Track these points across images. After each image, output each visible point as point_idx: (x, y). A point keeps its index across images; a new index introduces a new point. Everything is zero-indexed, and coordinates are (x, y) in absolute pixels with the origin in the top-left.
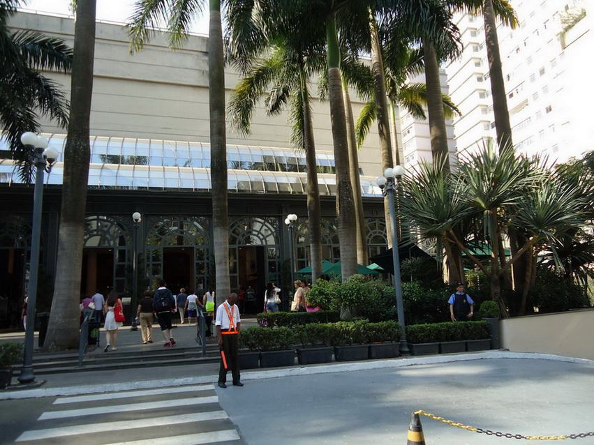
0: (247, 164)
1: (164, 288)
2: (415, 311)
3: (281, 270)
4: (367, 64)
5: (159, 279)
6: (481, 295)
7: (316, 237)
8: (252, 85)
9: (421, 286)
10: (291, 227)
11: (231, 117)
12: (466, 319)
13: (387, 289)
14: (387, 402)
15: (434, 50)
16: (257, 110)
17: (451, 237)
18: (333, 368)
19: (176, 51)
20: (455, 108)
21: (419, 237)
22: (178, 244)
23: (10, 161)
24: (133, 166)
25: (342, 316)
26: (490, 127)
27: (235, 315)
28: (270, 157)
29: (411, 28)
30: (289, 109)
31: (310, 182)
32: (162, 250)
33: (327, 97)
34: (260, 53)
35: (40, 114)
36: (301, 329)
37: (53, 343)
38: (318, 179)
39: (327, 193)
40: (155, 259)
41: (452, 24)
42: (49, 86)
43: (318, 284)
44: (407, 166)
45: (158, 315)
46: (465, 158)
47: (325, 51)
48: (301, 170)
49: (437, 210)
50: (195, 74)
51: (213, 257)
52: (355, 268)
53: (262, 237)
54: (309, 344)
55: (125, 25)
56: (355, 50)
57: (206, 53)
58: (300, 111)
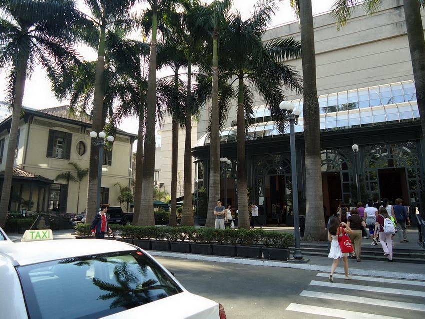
19: (373, 15)
22: (389, 166)
23: (272, 123)
35: (285, 90)
37: (309, 236)
42: (288, 70)
50: (389, 28)
55: (331, 12)
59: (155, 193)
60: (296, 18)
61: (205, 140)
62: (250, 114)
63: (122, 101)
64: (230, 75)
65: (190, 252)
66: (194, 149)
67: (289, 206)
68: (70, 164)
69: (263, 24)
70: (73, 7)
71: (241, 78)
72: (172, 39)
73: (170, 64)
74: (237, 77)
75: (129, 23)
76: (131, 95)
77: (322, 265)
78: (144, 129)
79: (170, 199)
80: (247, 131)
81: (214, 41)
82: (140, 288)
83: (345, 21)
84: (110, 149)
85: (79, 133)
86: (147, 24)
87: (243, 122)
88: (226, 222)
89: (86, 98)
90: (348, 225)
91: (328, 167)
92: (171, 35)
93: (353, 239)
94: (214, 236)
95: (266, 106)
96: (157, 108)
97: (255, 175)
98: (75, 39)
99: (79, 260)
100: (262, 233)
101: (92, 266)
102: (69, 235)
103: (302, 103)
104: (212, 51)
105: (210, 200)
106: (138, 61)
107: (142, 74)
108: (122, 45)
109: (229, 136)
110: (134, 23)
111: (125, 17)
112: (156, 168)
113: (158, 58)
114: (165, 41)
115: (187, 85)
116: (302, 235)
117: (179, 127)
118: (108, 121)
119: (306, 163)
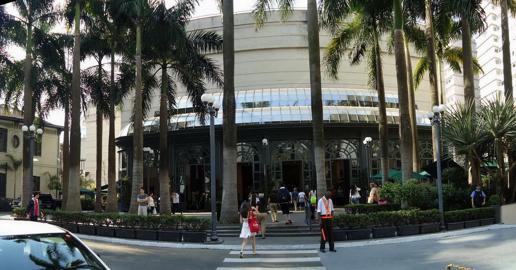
0: (336, 101)
1: (284, 188)
2: (450, 202)
3: (361, 176)
4: (422, 28)
5: (280, 182)
6: (490, 192)
7: (385, 153)
8: (339, 43)
9: (454, 186)
10: (367, 146)
11: (324, 68)
12: (481, 206)
13: (432, 188)
14: (430, 261)
15: (468, 25)
16: (343, 62)
17: (474, 155)
18: (396, 240)
19: (286, 23)
20: (480, 68)
21: (454, 154)
23: (194, 114)
24: (261, 108)
25: (403, 206)
26: (501, 84)
27: (330, 206)
28: (353, 96)
29: (453, 5)
30: (365, 61)
31: (381, 115)
32: (281, 163)
33: (393, 52)
34: (345, 18)
35: (207, 82)
36: (374, 216)
37: (225, 220)
38: (387, 112)
39: (393, 122)
40: (277, 169)
41: (481, 8)
42: (210, 63)
43: (386, 185)
44: (448, 105)
45: (280, 205)
46: (485, 103)
47: (392, 16)
48: (375, 106)
49: (466, 136)
50: (298, 38)
51: (315, 167)
52: (412, 175)
53: (347, 153)
54: (380, 225)
55: (251, 12)
56: (414, 17)
57: (306, 22)
58: (374, 61)
59: (81, 181)
60: (219, 12)
61: (129, 130)
62: (173, 105)
63: (49, 95)
64: (154, 64)
65: (115, 236)
66: (117, 139)
67: (207, 193)
68: (7, 155)
69: (187, 13)
70: (3, 12)
71: (164, 68)
72: (95, 28)
73: (94, 54)
74: (160, 66)
75: (53, 16)
76: (57, 88)
77: (234, 244)
78: (70, 121)
79: (95, 187)
80: (169, 121)
81: (138, 29)
82: (70, 266)
83: (262, 23)
84: (39, 141)
85: (12, 128)
86: (70, 16)
87: (166, 112)
88: (148, 208)
89: (17, 95)
90: (256, 209)
91: (243, 158)
92: (94, 24)
93: (260, 220)
94: (137, 222)
95: (189, 97)
96: (82, 99)
97: (177, 164)
98: (6, 41)
99: (17, 238)
100: (183, 219)
101: (28, 244)
102: (9, 216)
103: (222, 97)
104: (135, 39)
105: (134, 187)
106: (62, 53)
107: (66, 66)
108: (47, 40)
109: (152, 126)
110: (58, 15)
111: (49, 10)
112: (82, 157)
113: (81, 49)
114: (88, 30)
115: (110, 74)
116: (218, 219)
117: (103, 117)
118: (36, 115)
119: (224, 154)
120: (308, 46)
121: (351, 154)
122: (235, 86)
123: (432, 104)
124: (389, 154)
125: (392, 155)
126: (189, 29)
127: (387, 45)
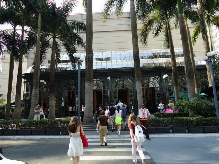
3: (162, 97)
4: (195, 10)
7: (176, 83)
10: (165, 80)
11: (140, 39)
13: (210, 103)
19: (119, 19)
25: (190, 114)
30: (162, 34)
35: (78, 47)
36: (172, 119)
40: (115, 93)
43: (178, 101)
48: (168, 57)
50: (125, 26)
52: (195, 95)
54: (176, 125)
56: (189, 5)
57: (129, 18)
58: (167, 33)
60: (85, 12)
64: (48, 35)
65: (17, 134)
66: (24, 74)
71: (54, 37)
74: (52, 37)
80: (56, 66)
81: (40, 15)
87: (55, 61)
94: (33, 124)
97: (60, 90)
100: (61, 121)
105: (32, 104)
109: (46, 68)
117: (15, 61)
120: (131, 29)
121: (156, 84)
122: (93, 49)
123: (205, 52)
124: (178, 84)
125: (181, 84)
126: (69, 19)
127: (174, 23)
